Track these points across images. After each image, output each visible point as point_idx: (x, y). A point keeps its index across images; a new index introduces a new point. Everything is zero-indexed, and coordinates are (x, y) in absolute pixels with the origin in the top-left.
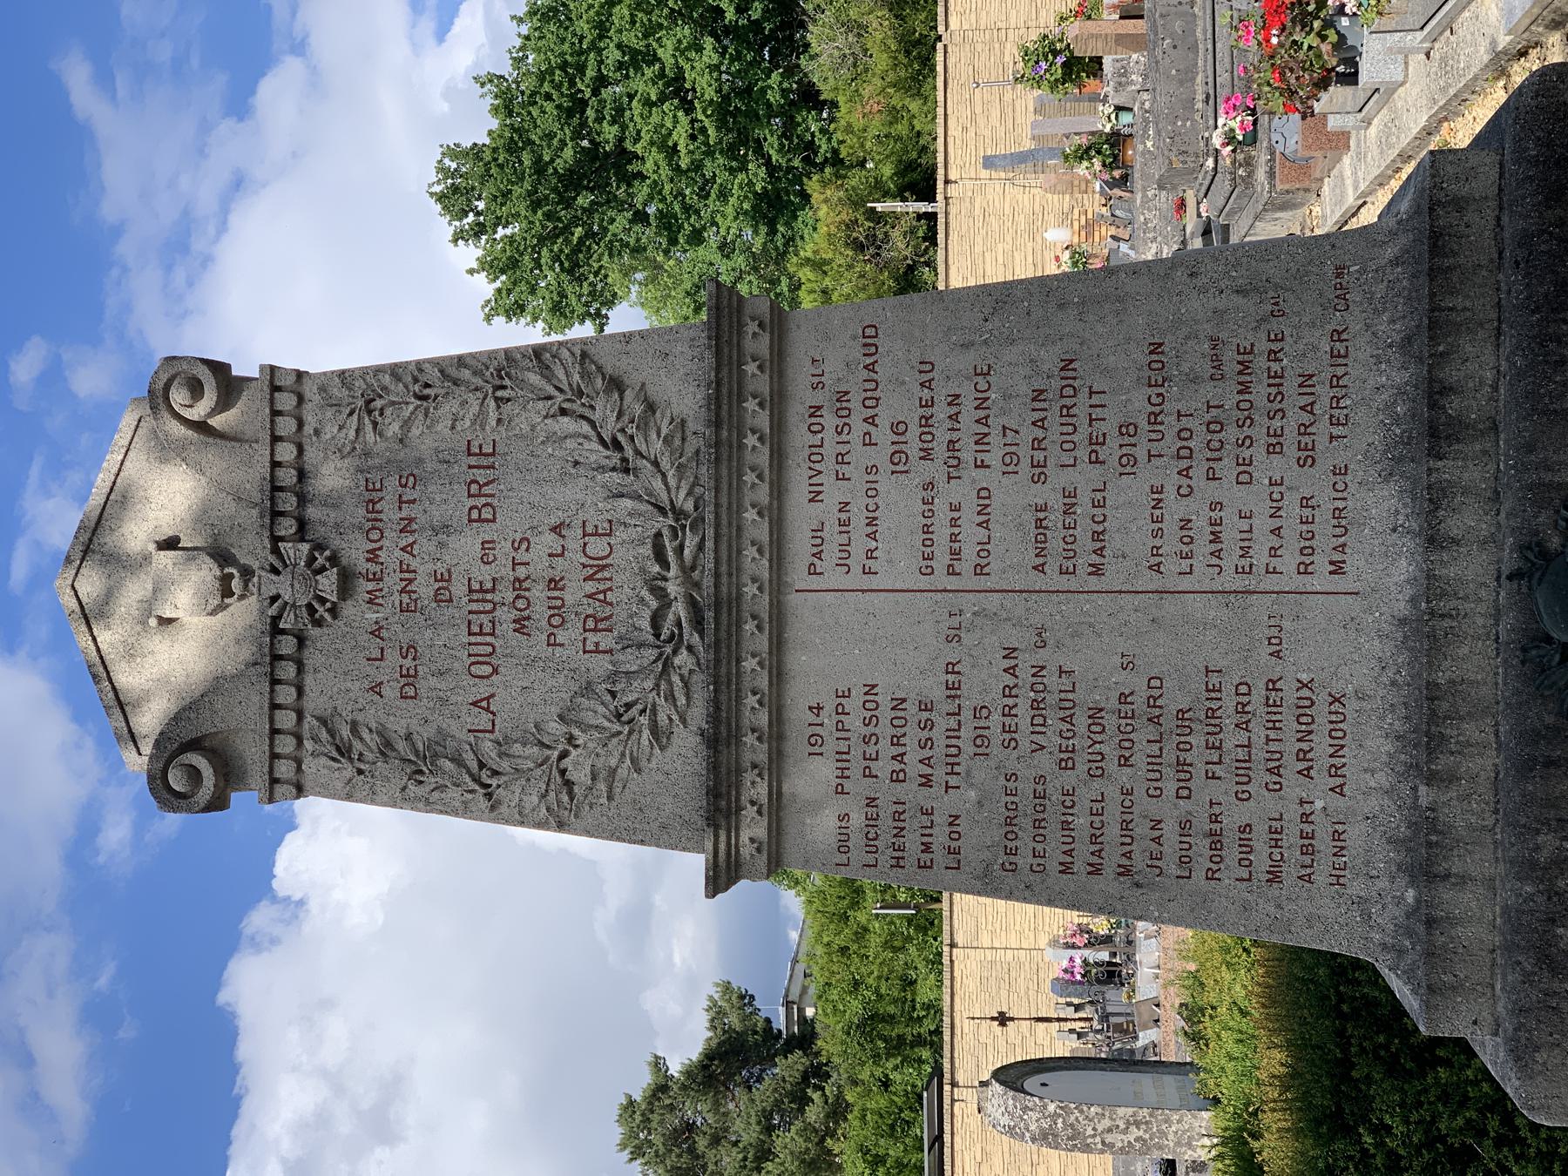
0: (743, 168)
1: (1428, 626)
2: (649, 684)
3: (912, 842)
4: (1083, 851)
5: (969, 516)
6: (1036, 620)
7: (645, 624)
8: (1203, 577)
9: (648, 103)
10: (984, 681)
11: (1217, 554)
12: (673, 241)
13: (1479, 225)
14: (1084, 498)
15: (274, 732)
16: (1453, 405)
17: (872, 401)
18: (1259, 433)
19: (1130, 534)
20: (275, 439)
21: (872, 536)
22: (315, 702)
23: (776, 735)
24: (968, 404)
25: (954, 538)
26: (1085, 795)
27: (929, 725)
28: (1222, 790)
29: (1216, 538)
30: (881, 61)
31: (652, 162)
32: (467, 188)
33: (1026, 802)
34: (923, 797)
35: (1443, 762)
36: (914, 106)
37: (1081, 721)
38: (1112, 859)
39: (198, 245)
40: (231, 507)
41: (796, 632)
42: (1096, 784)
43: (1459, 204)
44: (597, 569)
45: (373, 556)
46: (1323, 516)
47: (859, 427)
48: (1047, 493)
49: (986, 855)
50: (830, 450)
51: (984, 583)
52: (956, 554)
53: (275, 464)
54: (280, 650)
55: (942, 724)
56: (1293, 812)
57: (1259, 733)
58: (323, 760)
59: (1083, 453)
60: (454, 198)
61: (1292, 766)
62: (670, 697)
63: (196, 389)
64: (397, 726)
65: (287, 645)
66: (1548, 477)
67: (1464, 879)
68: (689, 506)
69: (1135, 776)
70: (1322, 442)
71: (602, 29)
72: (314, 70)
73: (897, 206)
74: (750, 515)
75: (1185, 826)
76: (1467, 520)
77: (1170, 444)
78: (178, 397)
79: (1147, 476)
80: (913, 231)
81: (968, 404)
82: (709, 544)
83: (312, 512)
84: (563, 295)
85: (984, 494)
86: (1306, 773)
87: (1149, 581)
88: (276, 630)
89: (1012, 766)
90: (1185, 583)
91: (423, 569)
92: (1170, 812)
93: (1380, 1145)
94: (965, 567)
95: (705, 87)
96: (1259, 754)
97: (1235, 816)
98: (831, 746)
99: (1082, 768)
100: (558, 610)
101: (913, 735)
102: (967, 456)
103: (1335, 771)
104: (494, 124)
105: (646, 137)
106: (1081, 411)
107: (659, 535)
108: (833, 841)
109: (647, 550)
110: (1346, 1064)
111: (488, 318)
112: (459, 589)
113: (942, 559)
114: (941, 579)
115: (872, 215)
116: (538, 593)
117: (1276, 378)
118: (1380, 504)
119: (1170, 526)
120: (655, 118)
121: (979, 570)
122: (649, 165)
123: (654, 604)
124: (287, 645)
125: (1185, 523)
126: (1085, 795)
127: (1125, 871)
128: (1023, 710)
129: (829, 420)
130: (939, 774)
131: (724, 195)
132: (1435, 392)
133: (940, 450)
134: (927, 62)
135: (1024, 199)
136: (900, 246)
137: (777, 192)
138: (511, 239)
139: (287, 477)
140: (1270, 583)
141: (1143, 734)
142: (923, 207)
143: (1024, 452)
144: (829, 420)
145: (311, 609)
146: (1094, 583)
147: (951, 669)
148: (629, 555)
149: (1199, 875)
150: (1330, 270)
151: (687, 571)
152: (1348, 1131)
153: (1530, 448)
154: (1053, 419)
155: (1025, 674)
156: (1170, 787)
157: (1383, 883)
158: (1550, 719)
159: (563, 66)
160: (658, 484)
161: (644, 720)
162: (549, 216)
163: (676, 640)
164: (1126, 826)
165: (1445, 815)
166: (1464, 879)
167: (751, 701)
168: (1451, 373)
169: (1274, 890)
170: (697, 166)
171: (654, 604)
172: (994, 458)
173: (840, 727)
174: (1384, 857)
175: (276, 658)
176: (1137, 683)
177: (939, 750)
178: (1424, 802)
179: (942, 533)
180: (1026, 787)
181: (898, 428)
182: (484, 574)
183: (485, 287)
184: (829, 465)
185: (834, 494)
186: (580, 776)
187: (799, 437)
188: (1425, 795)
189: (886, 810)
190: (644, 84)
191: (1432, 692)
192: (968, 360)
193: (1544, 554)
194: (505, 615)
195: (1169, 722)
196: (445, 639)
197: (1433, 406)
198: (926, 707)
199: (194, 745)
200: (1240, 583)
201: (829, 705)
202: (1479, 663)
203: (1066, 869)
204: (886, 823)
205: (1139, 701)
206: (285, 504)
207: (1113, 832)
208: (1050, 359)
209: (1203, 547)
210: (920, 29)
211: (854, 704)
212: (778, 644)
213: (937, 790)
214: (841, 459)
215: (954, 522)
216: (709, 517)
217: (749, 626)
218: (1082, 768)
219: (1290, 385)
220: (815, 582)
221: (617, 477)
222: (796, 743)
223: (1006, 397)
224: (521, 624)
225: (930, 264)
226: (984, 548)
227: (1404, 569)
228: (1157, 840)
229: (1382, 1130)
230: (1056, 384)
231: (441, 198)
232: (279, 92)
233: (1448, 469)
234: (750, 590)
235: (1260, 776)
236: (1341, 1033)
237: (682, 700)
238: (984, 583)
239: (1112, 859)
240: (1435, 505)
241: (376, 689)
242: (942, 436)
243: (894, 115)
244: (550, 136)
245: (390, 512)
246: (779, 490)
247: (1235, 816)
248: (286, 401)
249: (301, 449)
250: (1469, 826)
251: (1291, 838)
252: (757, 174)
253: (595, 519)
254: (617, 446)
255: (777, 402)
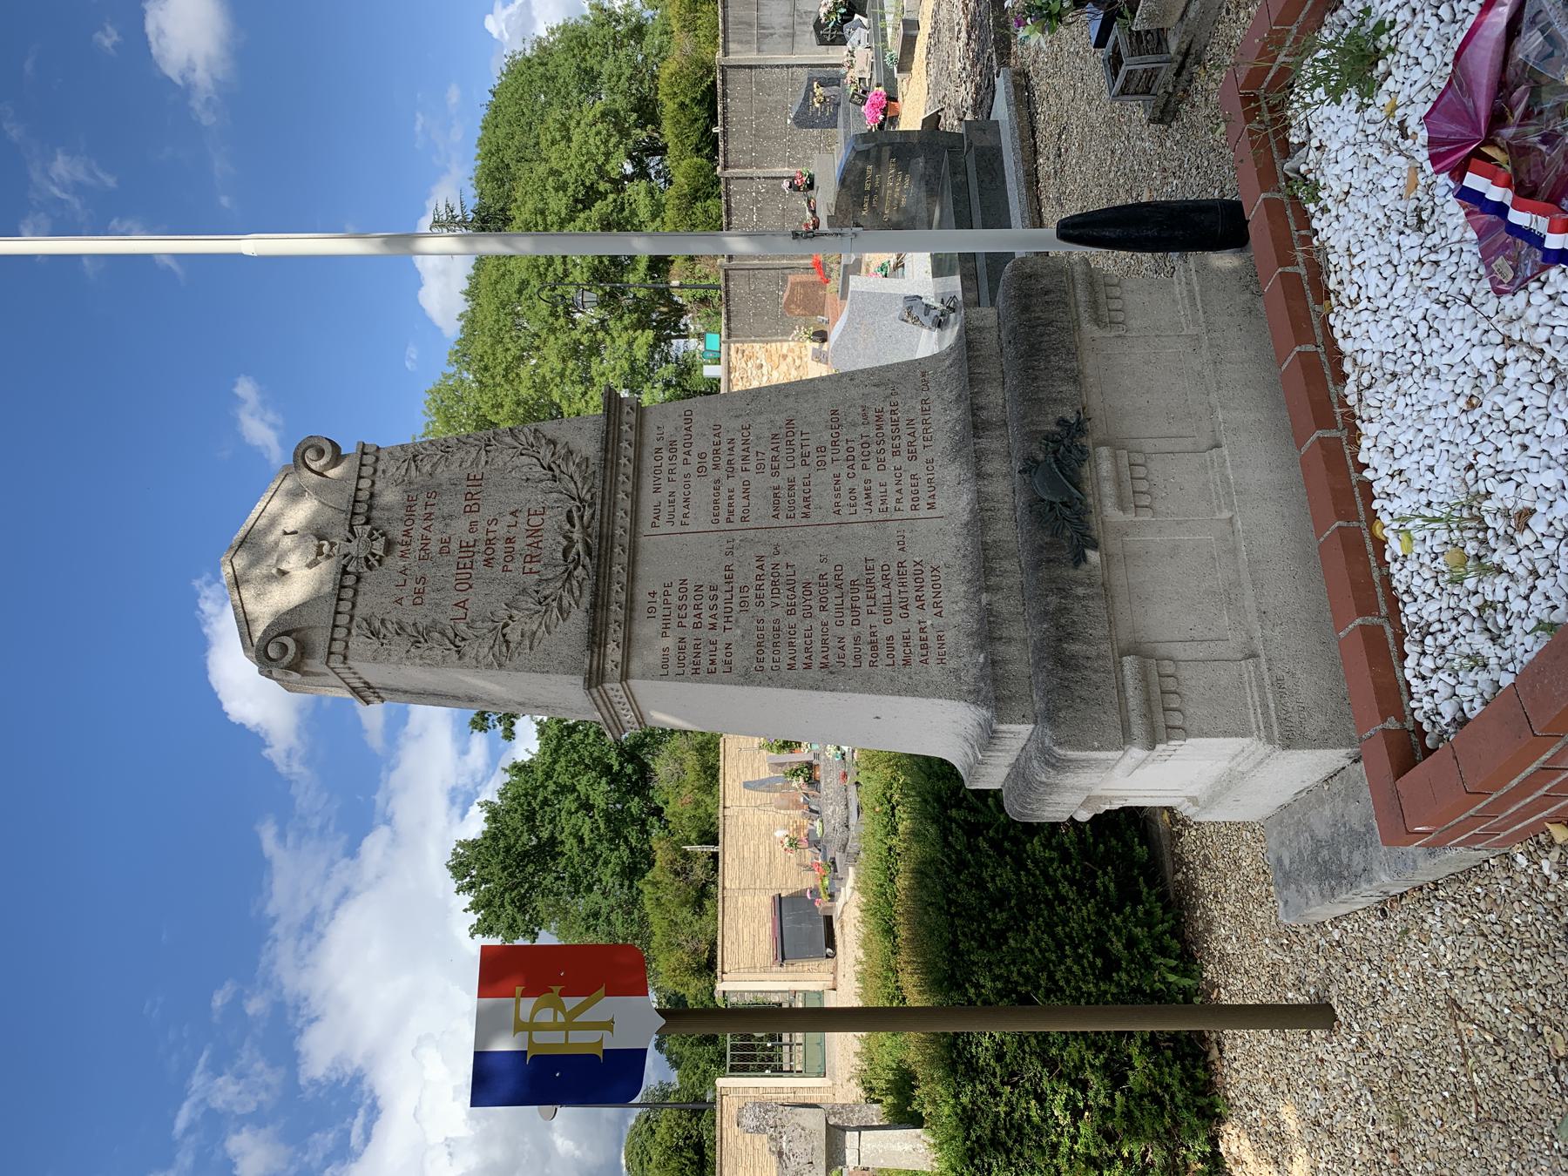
0: (617, 849)
1: (981, 518)
2: (559, 584)
3: (705, 660)
4: (801, 657)
5: (738, 493)
6: (775, 541)
7: (559, 555)
8: (862, 514)
9: (570, 813)
10: (745, 574)
11: (869, 504)
12: (577, 892)
13: (990, 338)
14: (799, 482)
15: (335, 626)
16: (984, 415)
17: (688, 444)
18: (888, 447)
19: (823, 497)
20: (360, 477)
21: (687, 507)
22: (360, 611)
23: (630, 606)
24: (739, 442)
25: (730, 505)
26: (802, 628)
27: (715, 597)
28: (876, 620)
29: (868, 496)
30: (691, 777)
31: (570, 845)
32: (467, 865)
33: (769, 634)
34: (712, 635)
35: (993, 580)
36: (708, 800)
37: (799, 590)
38: (817, 660)
39: (318, 927)
40: (329, 512)
41: (642, 556)
42: (808, 621)
43: (980, 330)
44: (535, 531)
45: (407, 533)
46: (923, 482)
47: (681, 456)
48: (780, 481)
49: (746, 663)
50: (665, 468)
51: (745, 525)
52: (731, 513)
53: (358, 489)
54: (346, 583)
55: (722, 596)
56: (915, 628)
57: (895, 589)
58: (362, 638)
59: (798, 461)
60: (459, 868)
61: (913, 604)
62: (571, 591)
63: (321, 453)
64: (408, 620)
65: (350, 580)
66: (1034, 428)
67: (1010, 640)
68: (588, 497)
69: (829, 616)
70: (920, 449)
71: (548, 776)
72: (394, 832)
73: (697, 848)
74: (621, 495)
75: (857, 639)
76: (994, 466)
77: (843, 454)
78: (310, 454)
79: (831, 470)
80: (706, 865)
81: (739, 442)
82: (597, 516)
83: (375, 514)
84: (515, 920)
85: (747, 484)
86: (921, 607)
87: (834, 519)
88: (345, 572)
89: (761, 615)
90: (853, 519)
91: (435, 537)
92: (848, 633)
93: (979, 995)
94: (736, 518)
95: (599, 801)
96: (895, 599)
97: (884, 632)
98: (660, 612)
99: (799, 614)
100: (510, 554)
101: (706, 603)
102: (738, 466)
103: (936, 605)
104: (485, 827)
105: (567, 831)
106: (797, 442)
107: (570, 511)
108: (659, 662)
109: (563, 517)
110: (954, 943)
111: (472, 936)
112: (454, 546)
113: (724, 515)
114: (723, 525)
115: (686, 855)
116: (500, 546)
117: (895, 422)
118: (951, 474)
119: (844, 492)
120: (573, 821)
121: (744, 519)
122: (568, 846)
123: (565, 543)
124: (350, 580)
125: (852, 491)
126: (802, 628)
127: (825, 666)
128: (767, 586)
129: (666, 454)
130: (720, 622)
131: (606, 863)
132: (975, 409)
133: (723, 463)
134: (715, 777)
135: (764, 817)
136: (699, 873)
137: (635, 863)
138: (489, 890)
139: (364, 495)
140: (897, 515)
141: (833, 594)
142: (712, 849)
143: (768, 462)
144: (666, 454)
145: (367, 560)
146: (804, 522)
147: (728, 568)
148: (554, 520)
149: (865, 664)
150: (919, 374)
151: (585, 528)
152: (960, 987)
153: (1024, 418)
154: (783, 446)
155: (768, 568)
156: (848, 620)
157: (966, 659)
158: (1047, 540)
159: (526, 795)
160: (572, 485)
161: (555, 604)
162: (511, 875)
163: (577, 563)
164: (824, 642)
165: (996, 606)
166: (1010, 640)
167: (616, 587)
168: (982, 401)
169: (908, 669)
170: (593, 849)
171: (565, 543)
172: (752, 467)
173: (666, 602)
174: (966, 643)
175: (342, 587)
176: (829, 569)
177: (721, 610)
178: (984, 602)
179: (724, 503)
180: (769, 626)
181: (702, 456)
182: (470, 538)
183: (473, 918)
184: (665, 475)
185: (666, 488)
186: (514, 637)
187: (649, 462)
188: (985, 598)
189: (690, 643)
190: (569, 803)
191: (985, 547)
192: (738, 423)
193: (1035, 461)
194: (479, 558)
195: (846, 587)
196: (445, 572)
197: (974, 415)
198: (713, 588)
199: (287, 633)
200: (882, 516)
201: (660, 592)
202: (1007, 532)
203: (791, 667)
204: (690, 651)
205: (830, 578)
206: (360, 510)
207: (817, 645)
208: (780, 420)
209: (862, 501)
210: (711, 761)
211: (673, 590)
212: (633, 562)
213: (719, 631)
214: (671, 472)
215: (730, 498)
216: (598, 501)
217: (617, 550)
218: (799, 614)
219: (903, 425)
220: (655, 531)
221: (549, 484)
222: (640, 613)
223: (758, 438)
224: (488, 563)
225: (715, 883)
226: (746, 509)
227: (965, 499)
228: (842, 648)
229: (978, 986)
230: (784, 431)
231: (452, 868)
232: (374, 846)
233: (984, 443)
234: (619, 532)
235: (897, 611)
236: (952, 925)
237: (577, 593)
238: (745, 525)
239: (817, 660)
240: (979, 459)
241: (399, 601)
242: (724, 458)
243: (698, 804)
244: (514, 830)
245: (419, 511)
246: (637, 487)
247: (884, 632)
248: (369, 459)
249: (373, 483)
250: (1011, 613)
251: (915, 640)
252: (624, 852)
253: (534, 506)
254: (551, 469)
255: (639, 445)
